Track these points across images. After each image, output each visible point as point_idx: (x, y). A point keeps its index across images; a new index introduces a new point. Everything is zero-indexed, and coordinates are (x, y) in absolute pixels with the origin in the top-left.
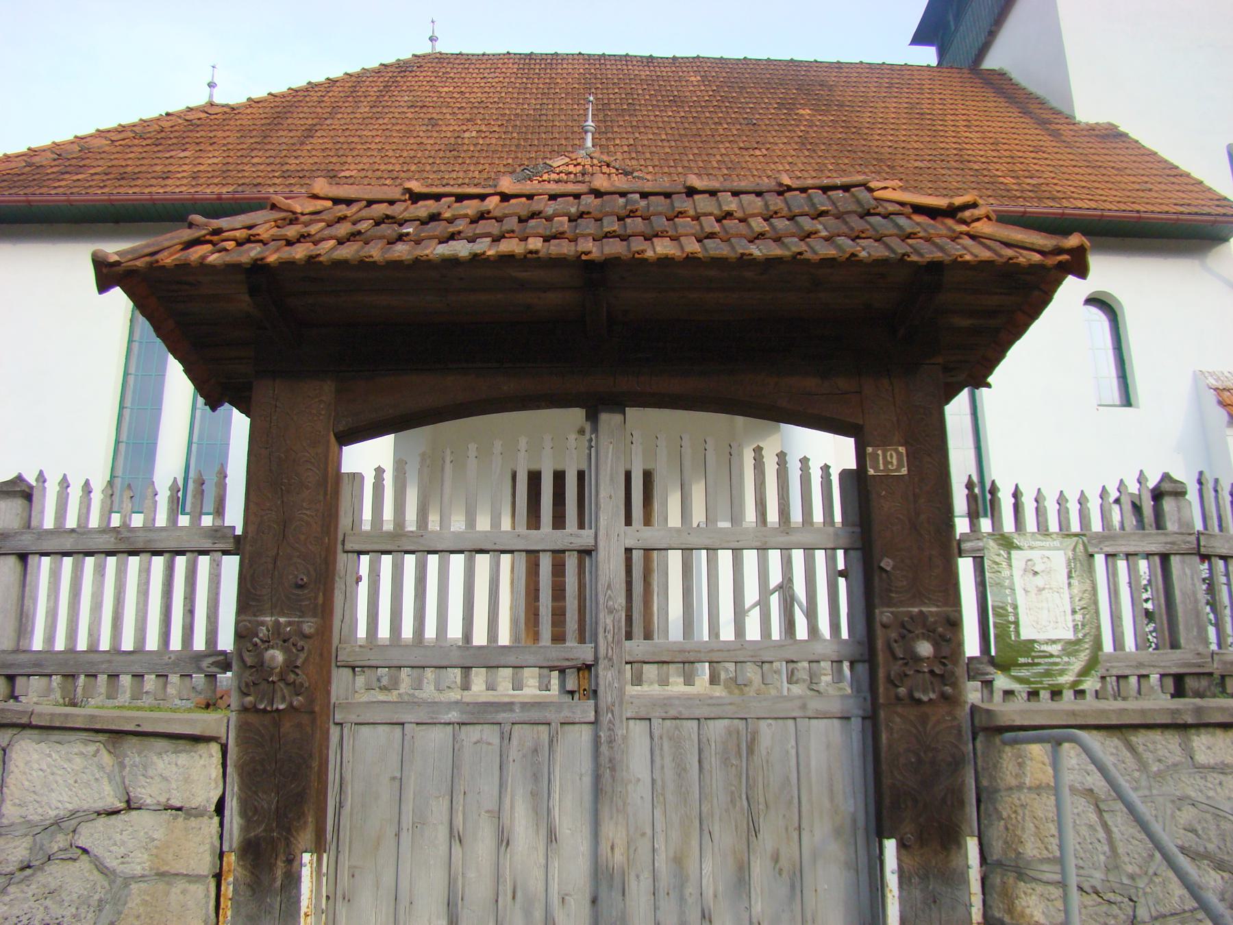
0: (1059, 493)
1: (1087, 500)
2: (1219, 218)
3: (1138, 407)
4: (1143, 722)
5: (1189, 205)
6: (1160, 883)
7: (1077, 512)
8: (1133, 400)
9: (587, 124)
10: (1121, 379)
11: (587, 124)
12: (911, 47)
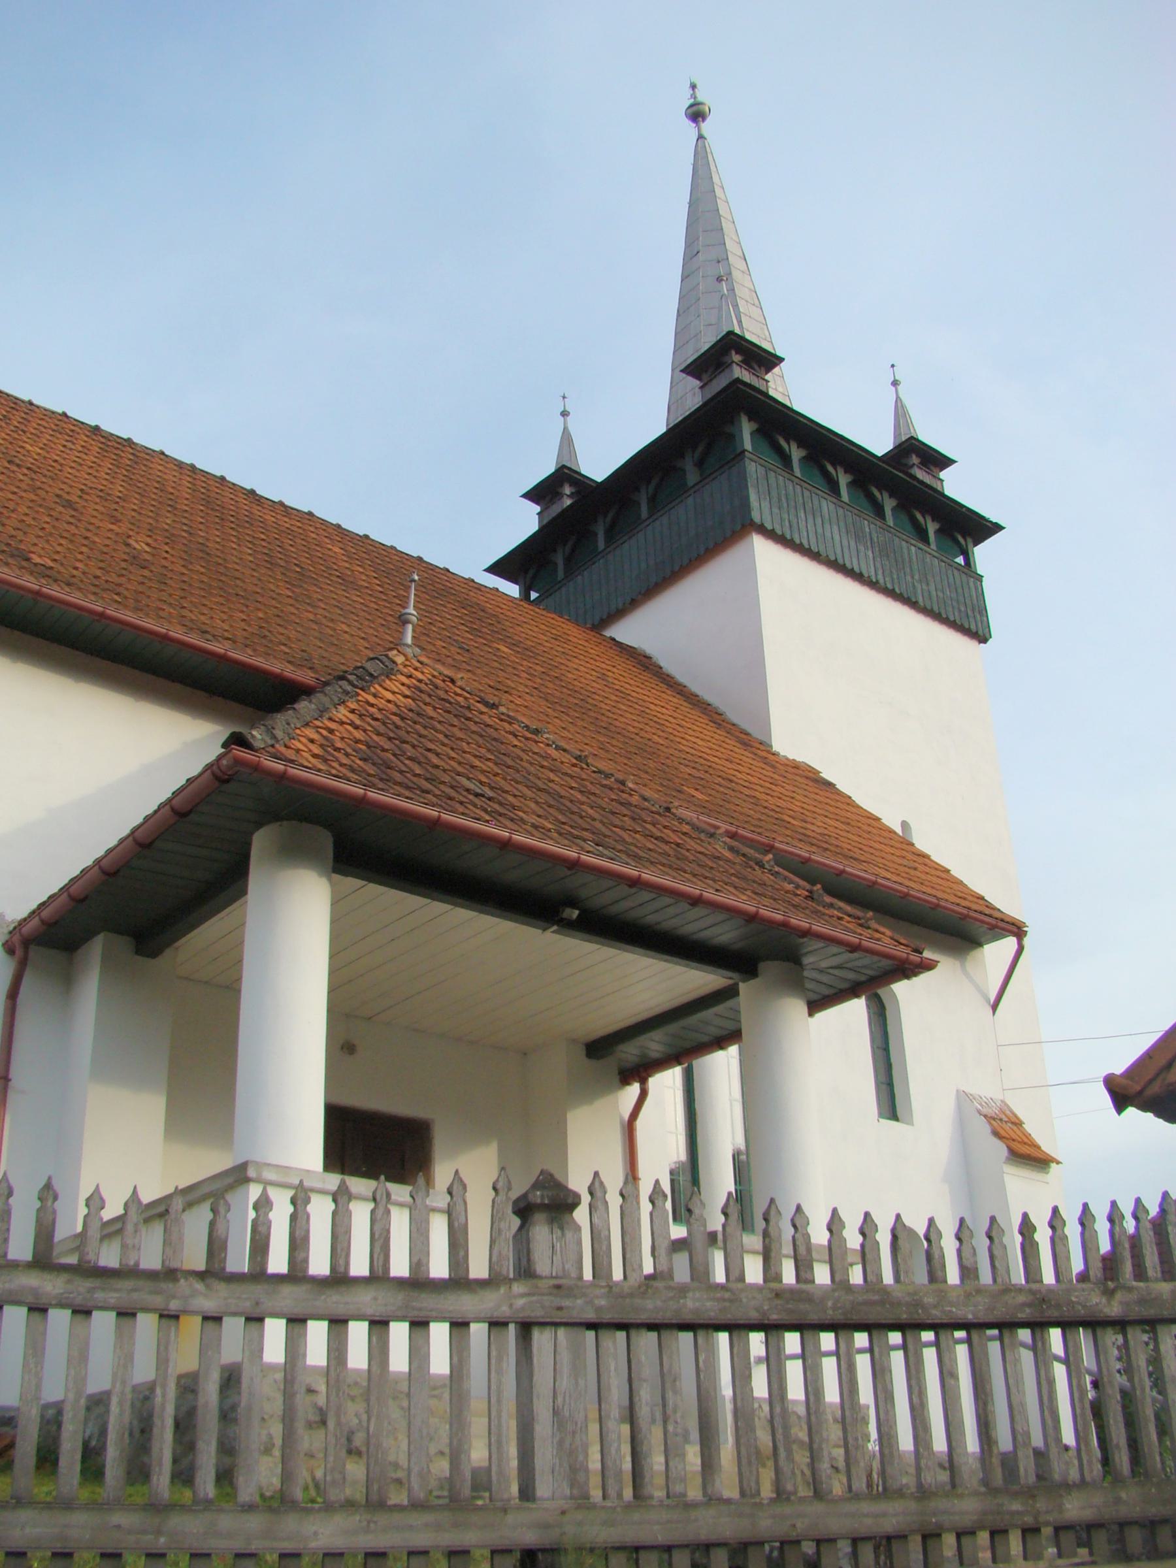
0: (1080, 1208)
1: (1034, 1229)
2: (972, 914)
3: (910, 1122)
4: (631, 1483)
5: (944, 892)
6: (175, 1554)
7: (1049, 1240)
8: (899, 1114)
9: (407, 611)
10: (884, 1087)
11: (407, 611)
12: (1003, 525)
